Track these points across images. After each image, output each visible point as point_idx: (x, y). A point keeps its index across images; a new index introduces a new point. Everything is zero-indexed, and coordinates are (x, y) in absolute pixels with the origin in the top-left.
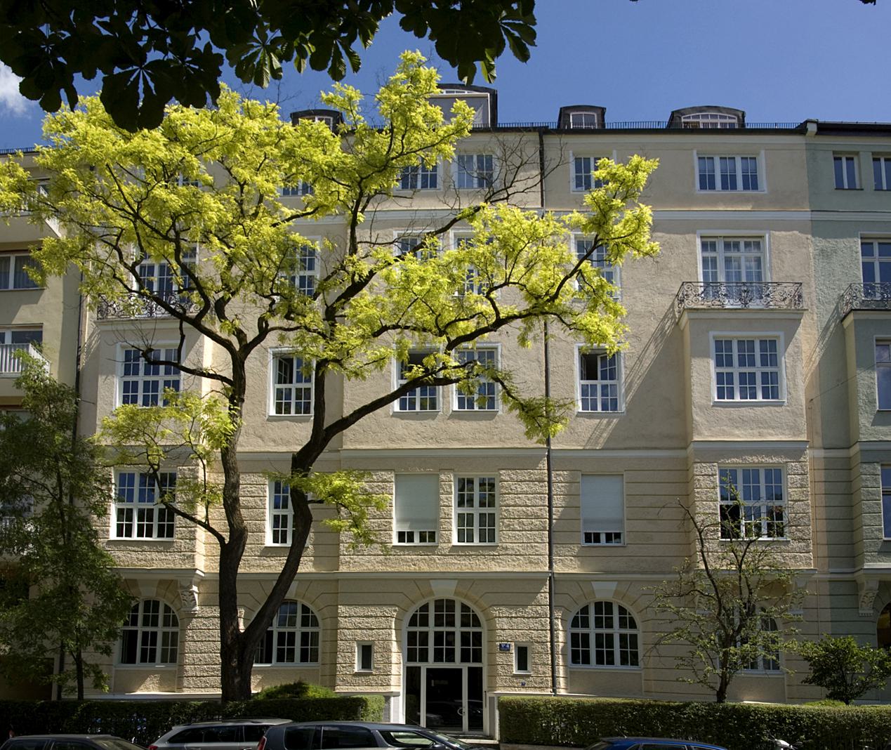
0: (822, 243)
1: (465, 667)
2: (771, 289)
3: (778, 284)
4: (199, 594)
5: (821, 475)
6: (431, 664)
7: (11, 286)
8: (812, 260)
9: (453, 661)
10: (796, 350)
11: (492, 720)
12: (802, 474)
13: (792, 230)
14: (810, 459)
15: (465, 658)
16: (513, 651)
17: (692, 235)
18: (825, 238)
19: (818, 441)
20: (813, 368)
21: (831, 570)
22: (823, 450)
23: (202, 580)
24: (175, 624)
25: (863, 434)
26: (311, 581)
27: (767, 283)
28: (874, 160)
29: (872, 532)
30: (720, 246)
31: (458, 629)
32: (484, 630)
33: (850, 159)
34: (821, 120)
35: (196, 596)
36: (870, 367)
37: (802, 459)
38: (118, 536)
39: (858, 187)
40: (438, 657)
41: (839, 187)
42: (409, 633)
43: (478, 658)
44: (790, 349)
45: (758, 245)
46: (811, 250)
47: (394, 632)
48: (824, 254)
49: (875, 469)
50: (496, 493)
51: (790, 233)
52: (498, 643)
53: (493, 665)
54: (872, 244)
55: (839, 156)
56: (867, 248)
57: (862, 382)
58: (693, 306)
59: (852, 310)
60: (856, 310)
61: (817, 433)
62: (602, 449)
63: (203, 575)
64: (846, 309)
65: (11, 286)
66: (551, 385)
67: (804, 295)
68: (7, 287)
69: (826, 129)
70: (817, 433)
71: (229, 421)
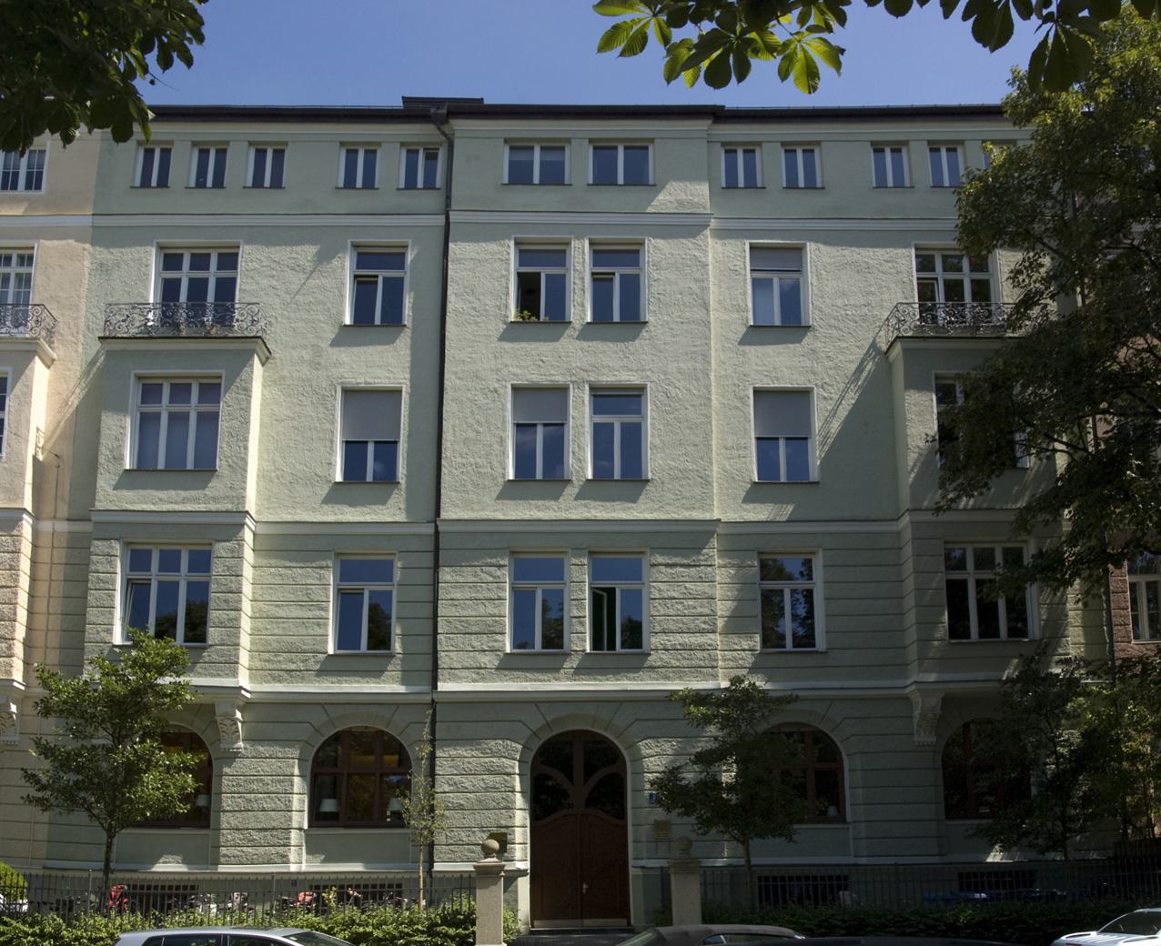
0: (104, 254)
4: (243, 723)
8: (87, 276)
10: (25, 389)
12: (13, 552)
13: (66, 239)
17: (150, 247)
18: (107, 247)
20: (68, 415)
22: (66, 522)
23: (247, 703)
25: (100, 501)
26: (398, 705)
28: (876, 151)
29: (98, 632)
35: (240, 725)
36: (121, 409)
37: (15, 532)
39: (566, 183)
44: (19, 385)
46: (87, 263)
47: (517, 778)
48: (102, 268)
49: (112, 547)
51: (64, 242)
55: (752, 148)
56: (925, 263)
57: (107, 432)
59: (897, 337)
60: (903, 337)
61: (63, 499)
62: (788, 521)
63: (248, 695)
65: (378, 321)
70: (63, 499)
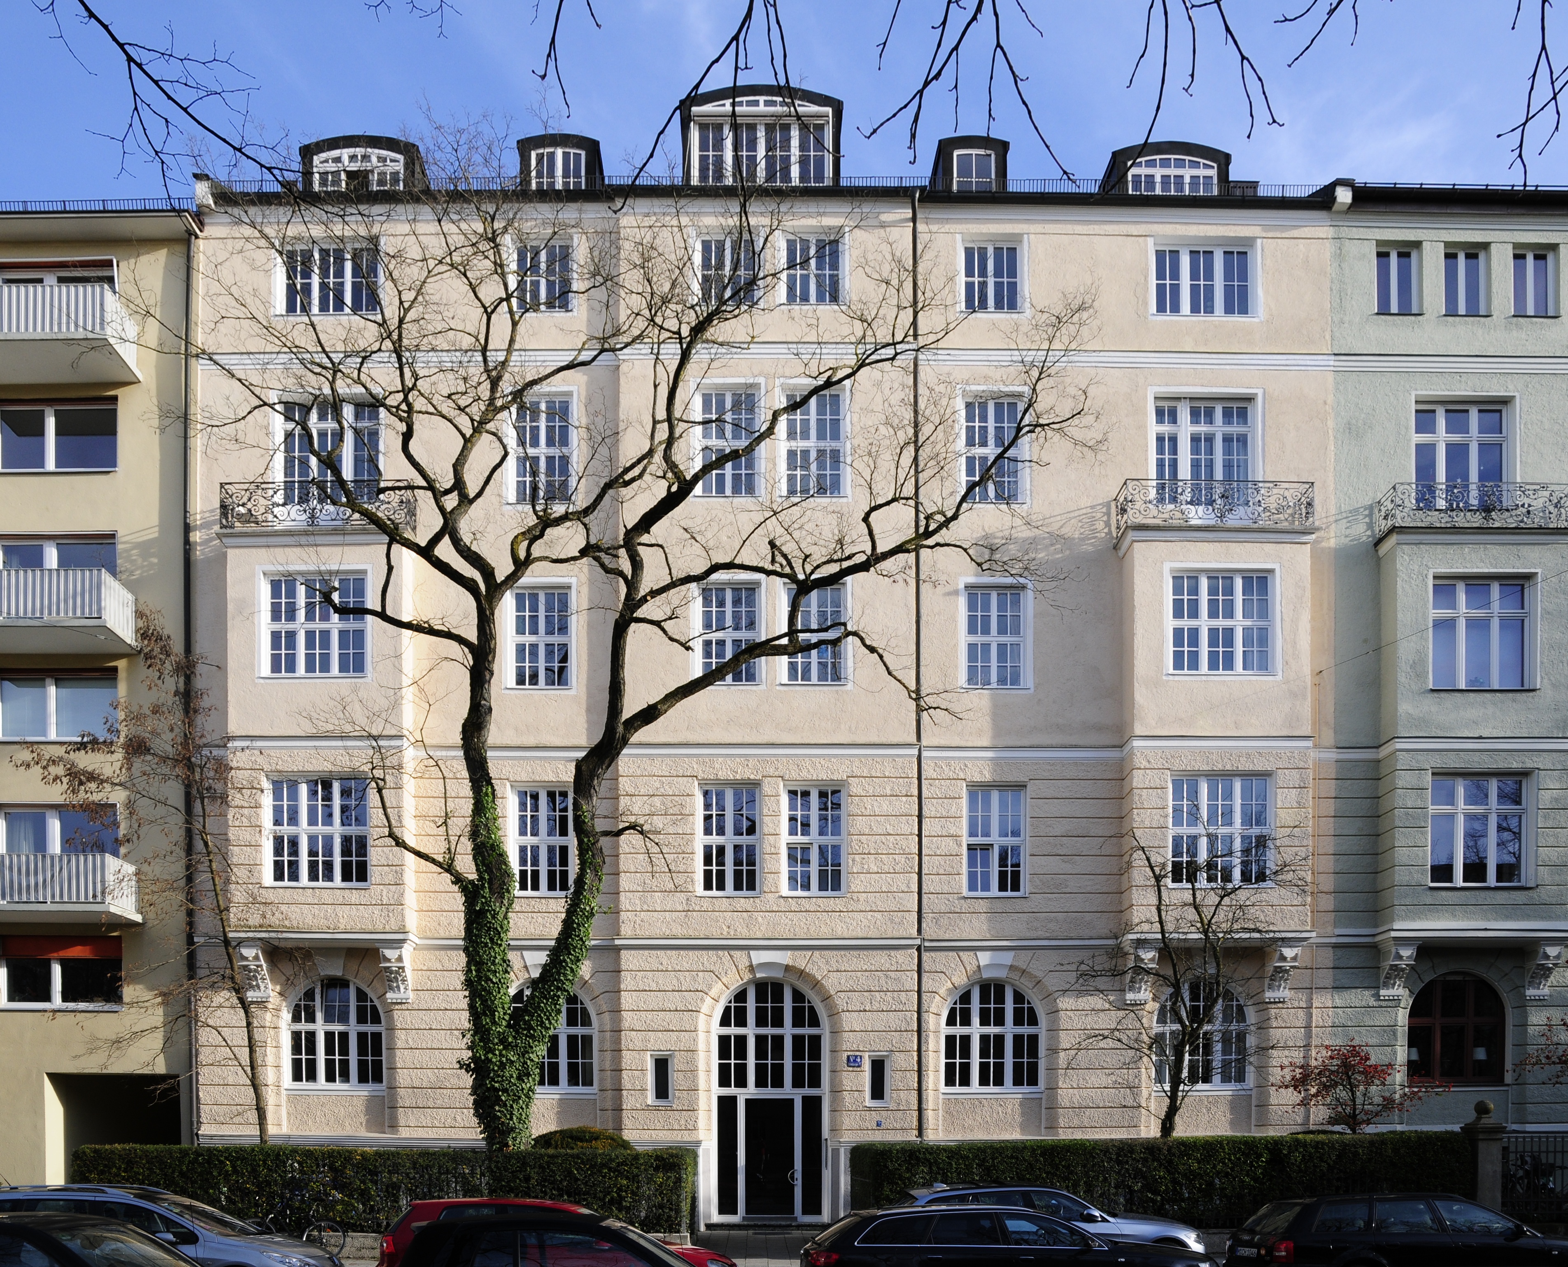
1: (797, 1096)
2: (1262, 491)
3: (1276, 484)
5: (1330, 787)
6: (751, 1091)
7: (50, 464)
9: (781, 1085)
11: (837, 1181)
14: (1314, 764)
15: (798, 1083)
16: (867, 1066)
19: (1328, 737)
21: (1338, 931)
24: (376, 1020)
27: (1255, 483)
30: (1184, 414)
31: (788, 1031)
32: (825, 1031)
33: (1404, 255)
34: (1360, 179)
38: (276, 879)
39: (1415, 310)
40: (761, 1082)
41: (1384, 310)
42: (721, 1099)
43: (815, 1082)
45: (1243, 414)
50: (843, 812)
52: (845, 1055)
53: (836, 1091)
54: (1434, 411)
58: (1140, 520)
64: (1384, 525)
66: (922, 611)
67: (1317, 503)
68: (41, 463)
69: (1373, 199)
71: (289, 233)
